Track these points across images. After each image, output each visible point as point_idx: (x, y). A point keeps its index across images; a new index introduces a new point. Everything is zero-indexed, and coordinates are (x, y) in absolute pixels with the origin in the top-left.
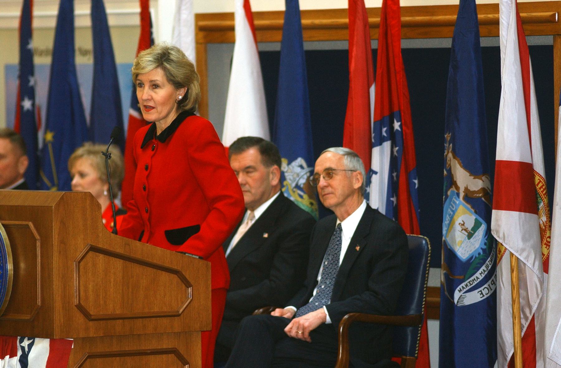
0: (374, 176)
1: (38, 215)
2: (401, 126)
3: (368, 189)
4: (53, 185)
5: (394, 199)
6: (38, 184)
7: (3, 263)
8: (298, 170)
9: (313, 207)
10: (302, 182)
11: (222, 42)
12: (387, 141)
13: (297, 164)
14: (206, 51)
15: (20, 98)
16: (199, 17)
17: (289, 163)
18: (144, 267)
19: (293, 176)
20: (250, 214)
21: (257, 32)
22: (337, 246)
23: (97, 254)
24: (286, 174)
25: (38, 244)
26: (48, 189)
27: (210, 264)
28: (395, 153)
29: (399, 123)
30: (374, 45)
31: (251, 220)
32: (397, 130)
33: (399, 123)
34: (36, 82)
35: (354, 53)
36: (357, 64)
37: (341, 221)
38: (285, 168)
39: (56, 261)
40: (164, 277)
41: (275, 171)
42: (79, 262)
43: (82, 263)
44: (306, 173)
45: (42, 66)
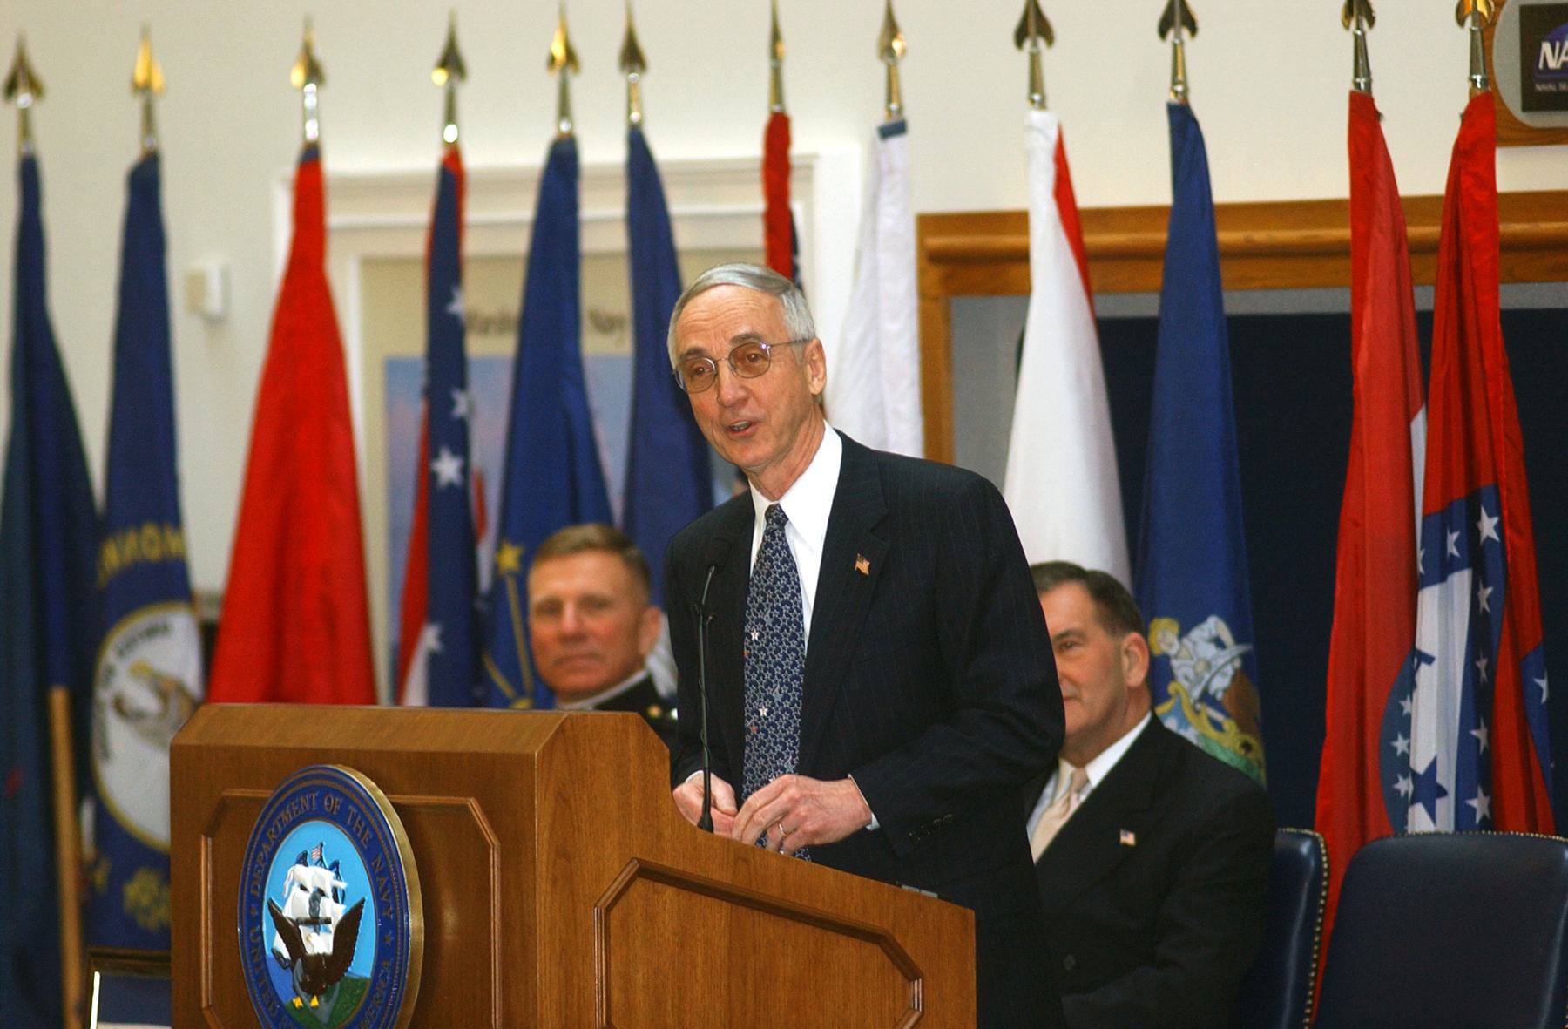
0: (1424, 667)
1: (493, 778)
2: (1499, 528)
3: (1406, 705)
4: (521, 692)
5: (1480, 734)
6: (479, 692)
7: (394, 912)
8: (1210, 651)
9: (1251, 756)
10: (1220, 684)
11: (994, 292)
12: (1460, 568)
13: (1206, 635)
14: (947, 319)
15: (429, 452)
16: (929, 224)
17: (1184, 632)
18: (789, 922)
19: (1194, 667)
20: (1072, 777)
21: (1092, 266)
22: (784, 580)
23: (659, 886)
24: (1175, 663)
25: (494, 859)
26: (505, 703)
27: (971, 914)
28: (1484, 604)
29: (1495, 520)
30: (1425, 298)
31: (1079, 791)
32: (1488, 538)
33: (1495, 520)
34: (471, 407)
35: (1366, 326)
36: (1374, 356)
37: (783, 489)
38: (1170, 645)
39: (544, 906)
40: (846, 951)
41: (1135, 649)
42: (608, 910)
43: (615, 911)
44: (1231, 661)
45: (490, 363)
